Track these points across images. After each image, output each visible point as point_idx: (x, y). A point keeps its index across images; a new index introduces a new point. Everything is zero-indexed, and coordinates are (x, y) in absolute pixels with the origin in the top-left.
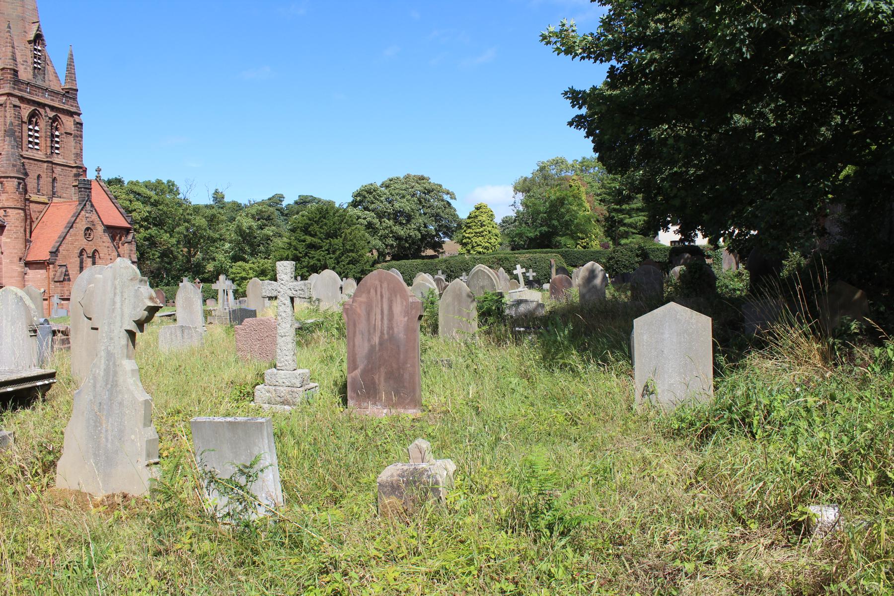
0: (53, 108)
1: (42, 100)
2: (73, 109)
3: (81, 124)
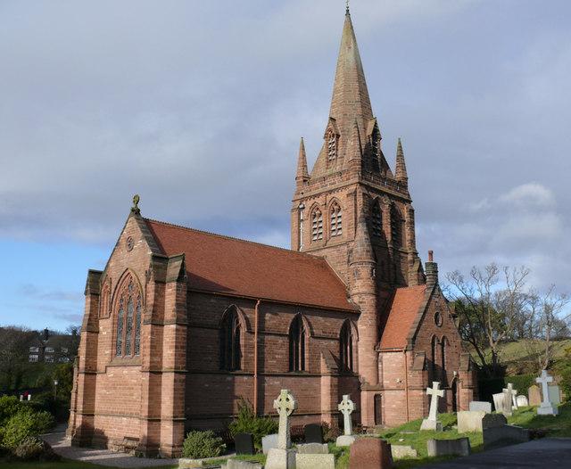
0: (390, 196)
1: (317, 192)
2: (406, 197)
3: (413, 211)
